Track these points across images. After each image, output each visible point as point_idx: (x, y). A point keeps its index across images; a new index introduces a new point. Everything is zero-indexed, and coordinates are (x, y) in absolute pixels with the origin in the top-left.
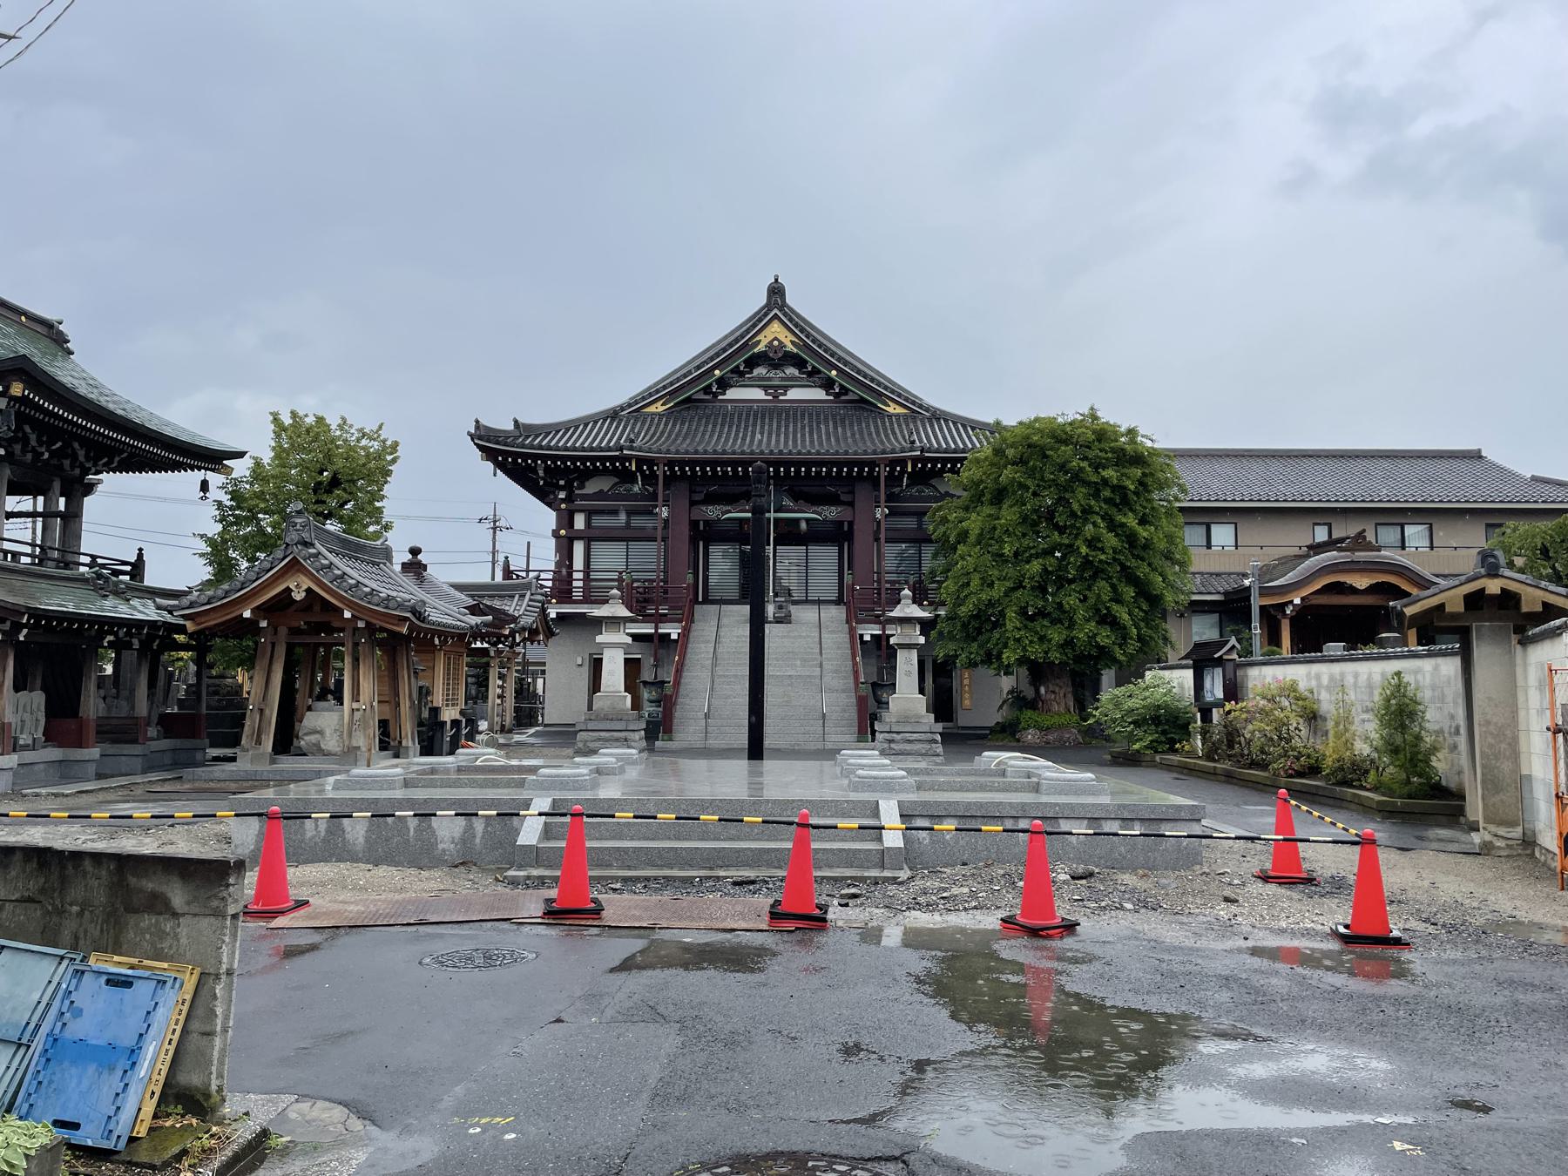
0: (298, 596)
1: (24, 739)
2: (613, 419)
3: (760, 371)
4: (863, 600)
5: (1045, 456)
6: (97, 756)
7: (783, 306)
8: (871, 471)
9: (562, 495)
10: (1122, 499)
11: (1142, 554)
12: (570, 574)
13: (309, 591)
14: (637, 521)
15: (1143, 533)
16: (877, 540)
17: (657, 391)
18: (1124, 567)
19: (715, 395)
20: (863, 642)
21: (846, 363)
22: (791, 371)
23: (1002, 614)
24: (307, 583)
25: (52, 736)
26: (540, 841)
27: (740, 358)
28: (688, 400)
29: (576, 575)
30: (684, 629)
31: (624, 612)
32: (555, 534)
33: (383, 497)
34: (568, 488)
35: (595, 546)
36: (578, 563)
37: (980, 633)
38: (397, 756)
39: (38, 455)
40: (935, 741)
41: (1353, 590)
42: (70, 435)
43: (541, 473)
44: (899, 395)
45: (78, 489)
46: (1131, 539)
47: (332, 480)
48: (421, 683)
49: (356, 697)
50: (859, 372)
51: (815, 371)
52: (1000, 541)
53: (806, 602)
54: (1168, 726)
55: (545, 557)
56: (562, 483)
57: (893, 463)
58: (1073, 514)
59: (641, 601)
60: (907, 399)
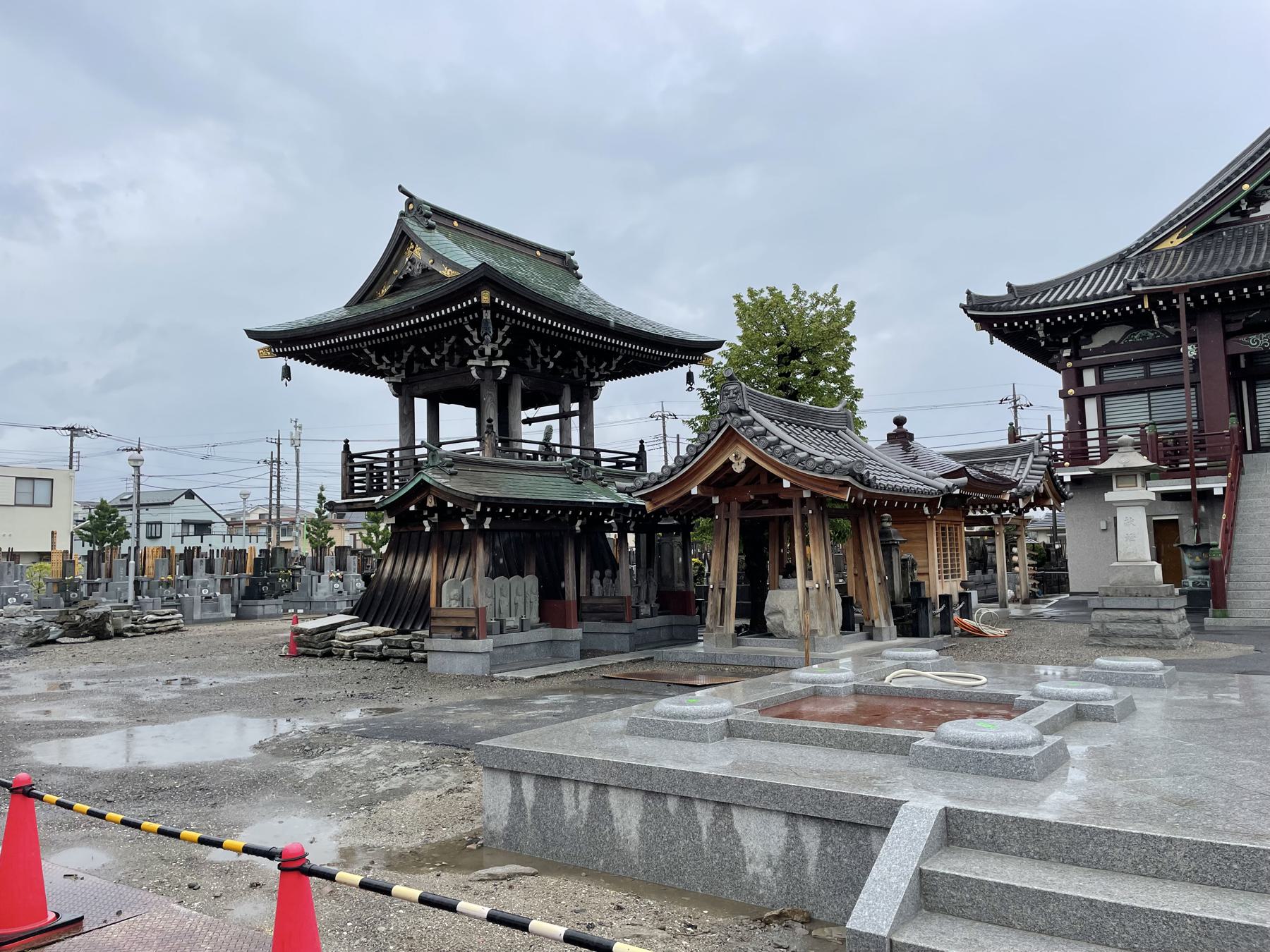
0: (739, 468)
1: (512, 622)
2: (1119, 264)
6: (580, 636)
9: (1067, 353)
12: (1084, 434)
13: (748, 461)
14: (1158, 369)
17: (1171, 224)
19: (1245, 214)
24: (745, 454)
25: (546, 617)
26: (902, 920)
28: (1212, 226)
29: (1090, 435)
30: (1231, 482)
31: (1143, 462)
32: (1063, 395)
33: (850, 364)
34: (1075, 345)
35: (1109, 401)
38: (870, 638)
39: (545, 365)
42: (570, 347)
43: (1041, 334)
45: (586, 395)
47: (796, 354)
48: (906, 556)
49: (808, 574)
56: (1065, 340)
59: (1168, 454)
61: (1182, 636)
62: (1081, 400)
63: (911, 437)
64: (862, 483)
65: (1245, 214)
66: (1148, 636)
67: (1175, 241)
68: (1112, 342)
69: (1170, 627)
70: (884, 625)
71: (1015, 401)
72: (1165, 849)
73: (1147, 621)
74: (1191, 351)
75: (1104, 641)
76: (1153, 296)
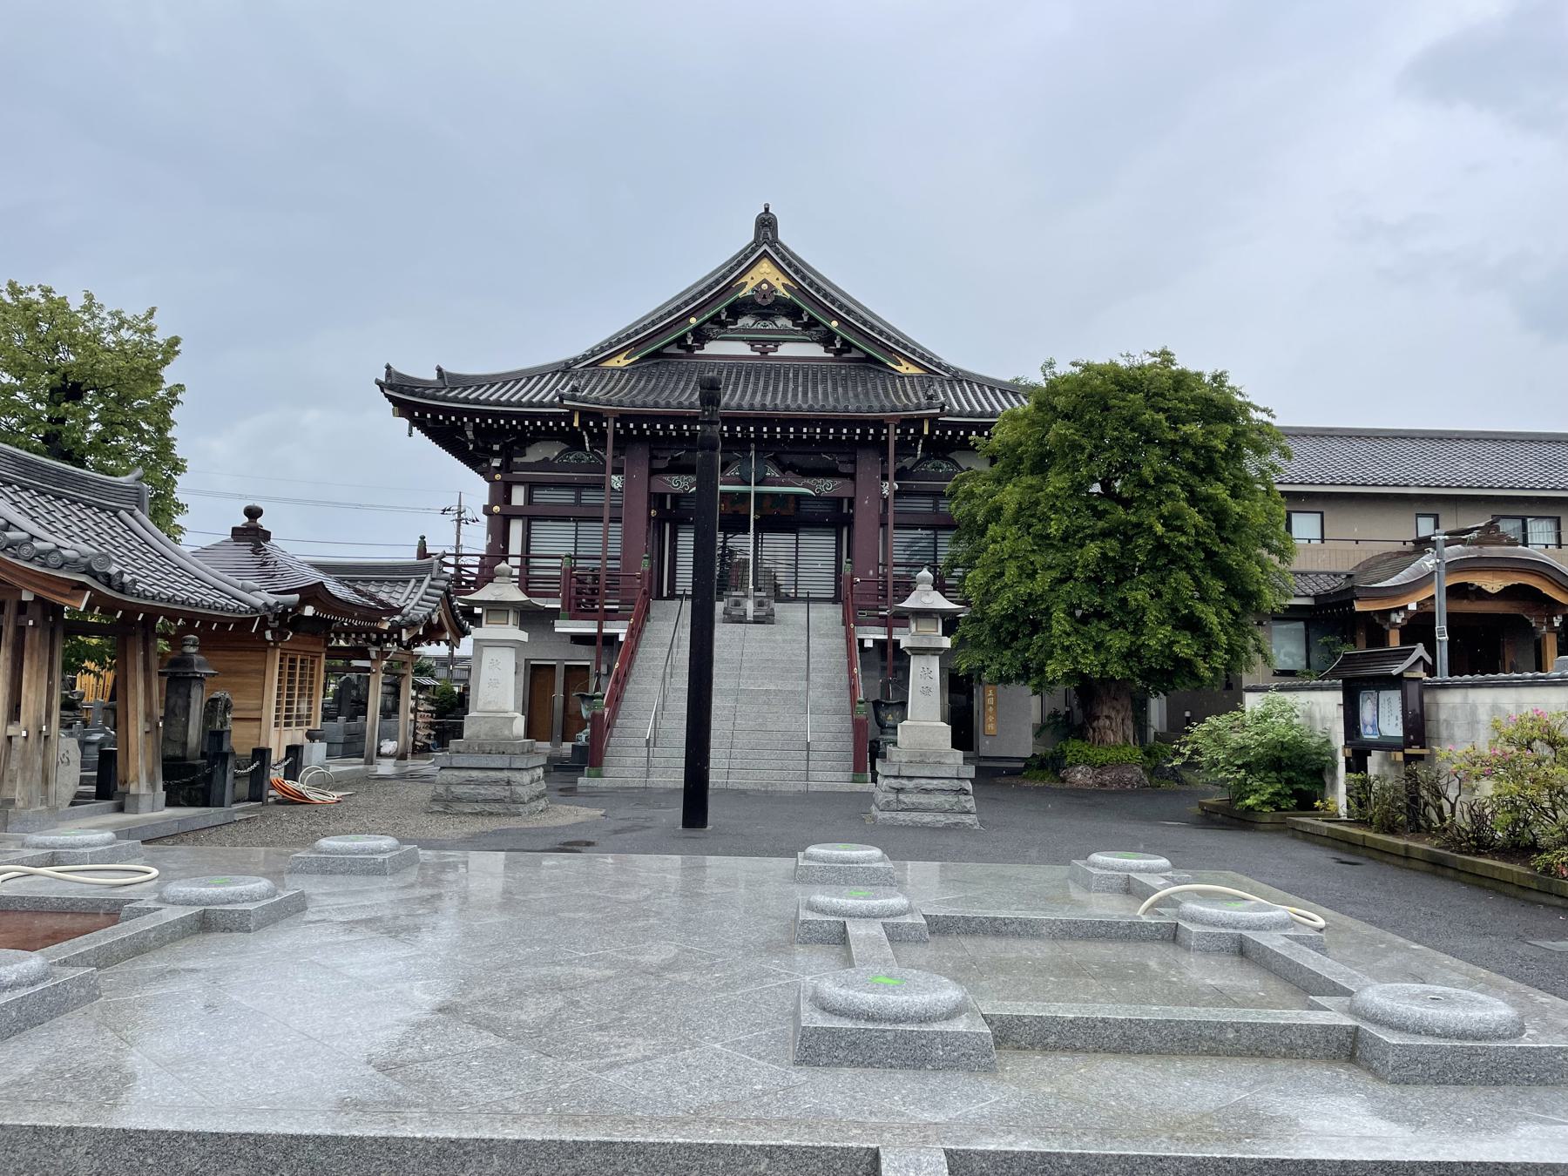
2: (564, 373)
3: (746, 321)
4: (865, 597)
5: (1106, 408)
7: (774, 242)
8: (878, 433)
9: (496, 463)
10: (1207, 465)
11: (1231, 536)
14: (589, 497)
15: (1236, 507)
16: (884, 525)
17: (619, 341)
18: (1210, 555)
19: (690, 349)
20: (863, 649)
21: (849, 312)
22: (784, 322)
23: (1047, 613)
27: (723, 304)
28: (657, 354)
32: (487, 510)
34: (507, 454)
36: (515, 546)
37: (1014, 636)
38: (120, 809)
40: (966, 793)
41: (1480, 594)
43: (470, 434)
44: (913, 352)
46: (1219, 517)
50: (865, 323)
51: (813, 323)
52: (1045, 519)
53: (796, 599)
54: (1295, 772)
56: (496, 447)
57: (905, 423)
58: (1143, 484)
60: (922, 357)
61: (531, 800)
63: (267, 536)
64: (109, 585)
65: (690, 349)
66: (496, 801)
67: (621, 362)
68: (546, 459)
69: (519, 790)
70: (143, 790)
71: (460, 513)
72: (63, 1146)
73: (496, 782)
74: (616, 481)
75: (447, 807)
76: (586, 415)
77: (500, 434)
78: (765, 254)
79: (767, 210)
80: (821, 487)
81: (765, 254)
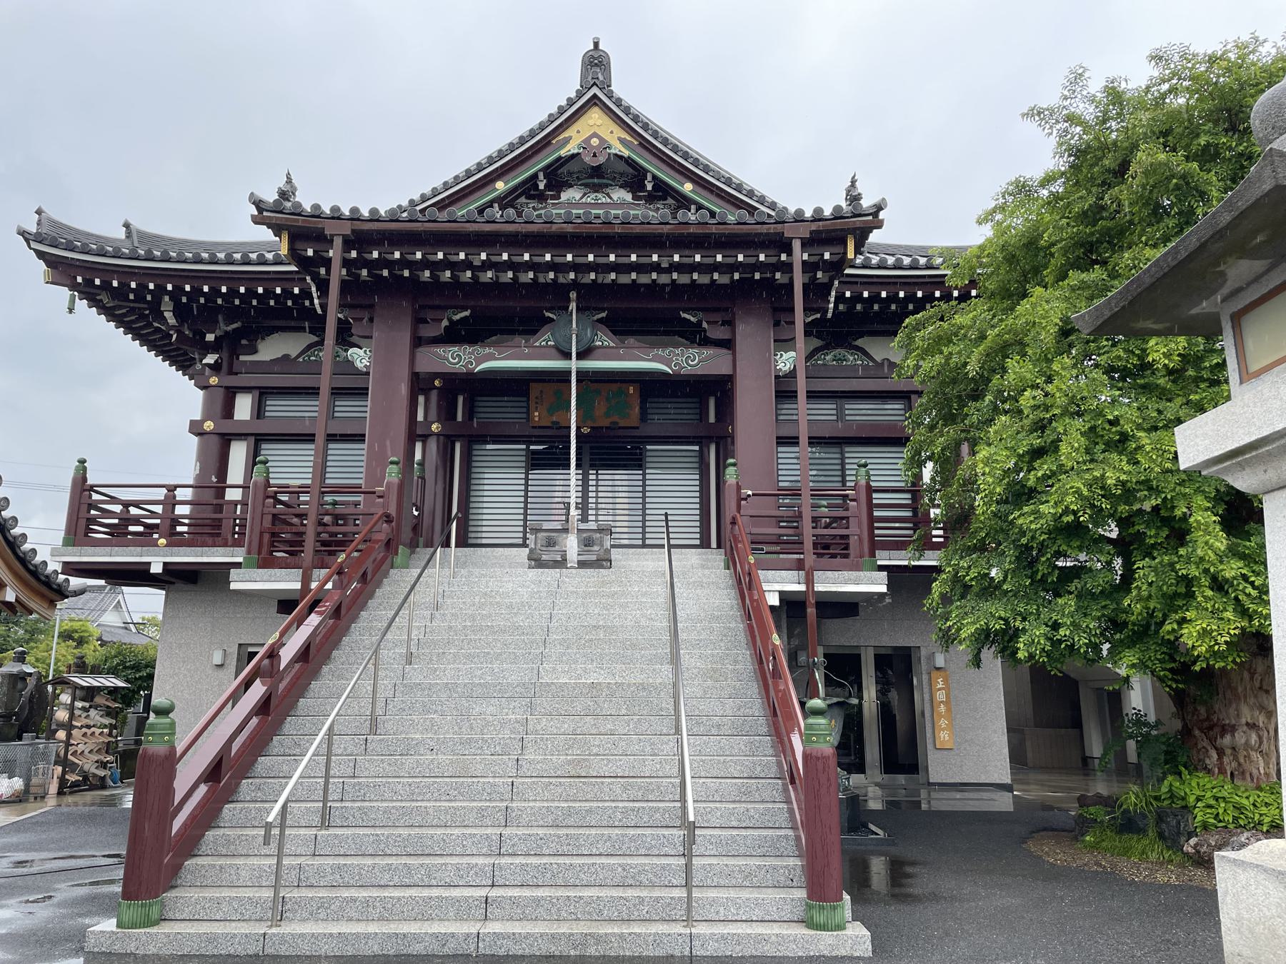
7: (606, 85)
9: (210, 359)
27: (540, 166)
35: (268, 450)
43: (171, 320)
55: (181, 464)
56: (210, 337)
62: (226, 440)
77: (209, 314)
78: (594, 100)
79: (596, 45)
80: (682, 360)
81: (594, 100)
